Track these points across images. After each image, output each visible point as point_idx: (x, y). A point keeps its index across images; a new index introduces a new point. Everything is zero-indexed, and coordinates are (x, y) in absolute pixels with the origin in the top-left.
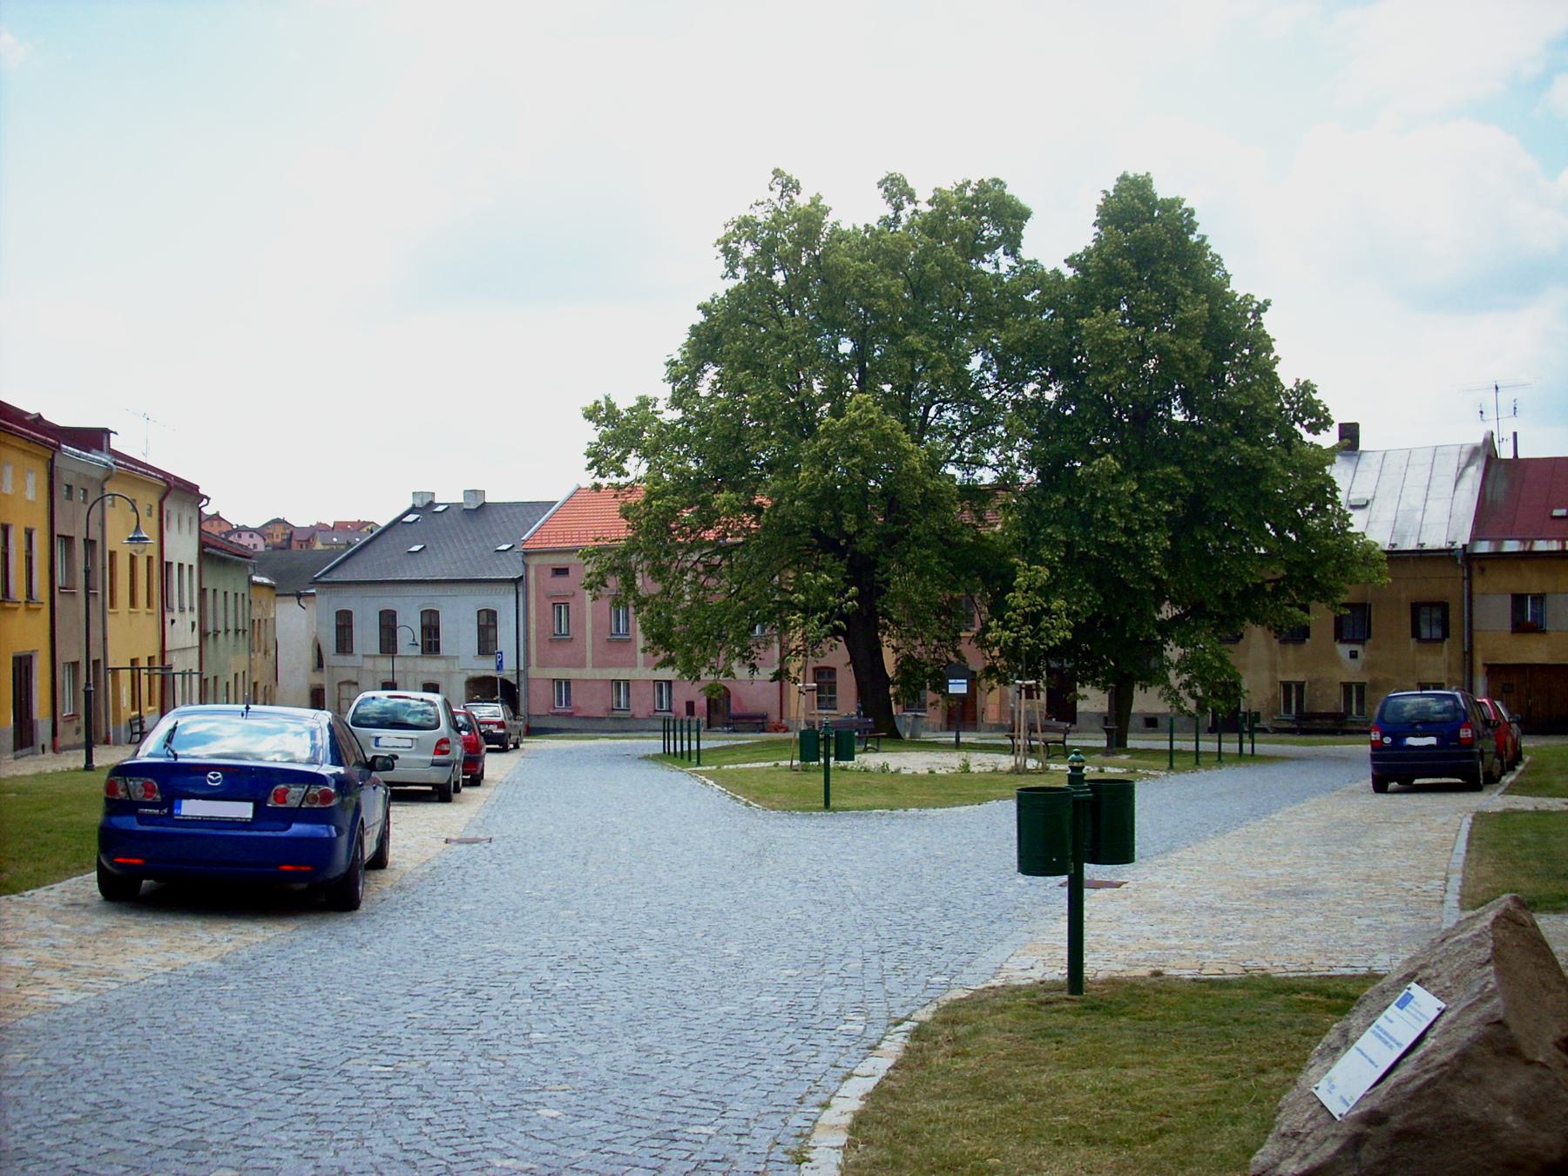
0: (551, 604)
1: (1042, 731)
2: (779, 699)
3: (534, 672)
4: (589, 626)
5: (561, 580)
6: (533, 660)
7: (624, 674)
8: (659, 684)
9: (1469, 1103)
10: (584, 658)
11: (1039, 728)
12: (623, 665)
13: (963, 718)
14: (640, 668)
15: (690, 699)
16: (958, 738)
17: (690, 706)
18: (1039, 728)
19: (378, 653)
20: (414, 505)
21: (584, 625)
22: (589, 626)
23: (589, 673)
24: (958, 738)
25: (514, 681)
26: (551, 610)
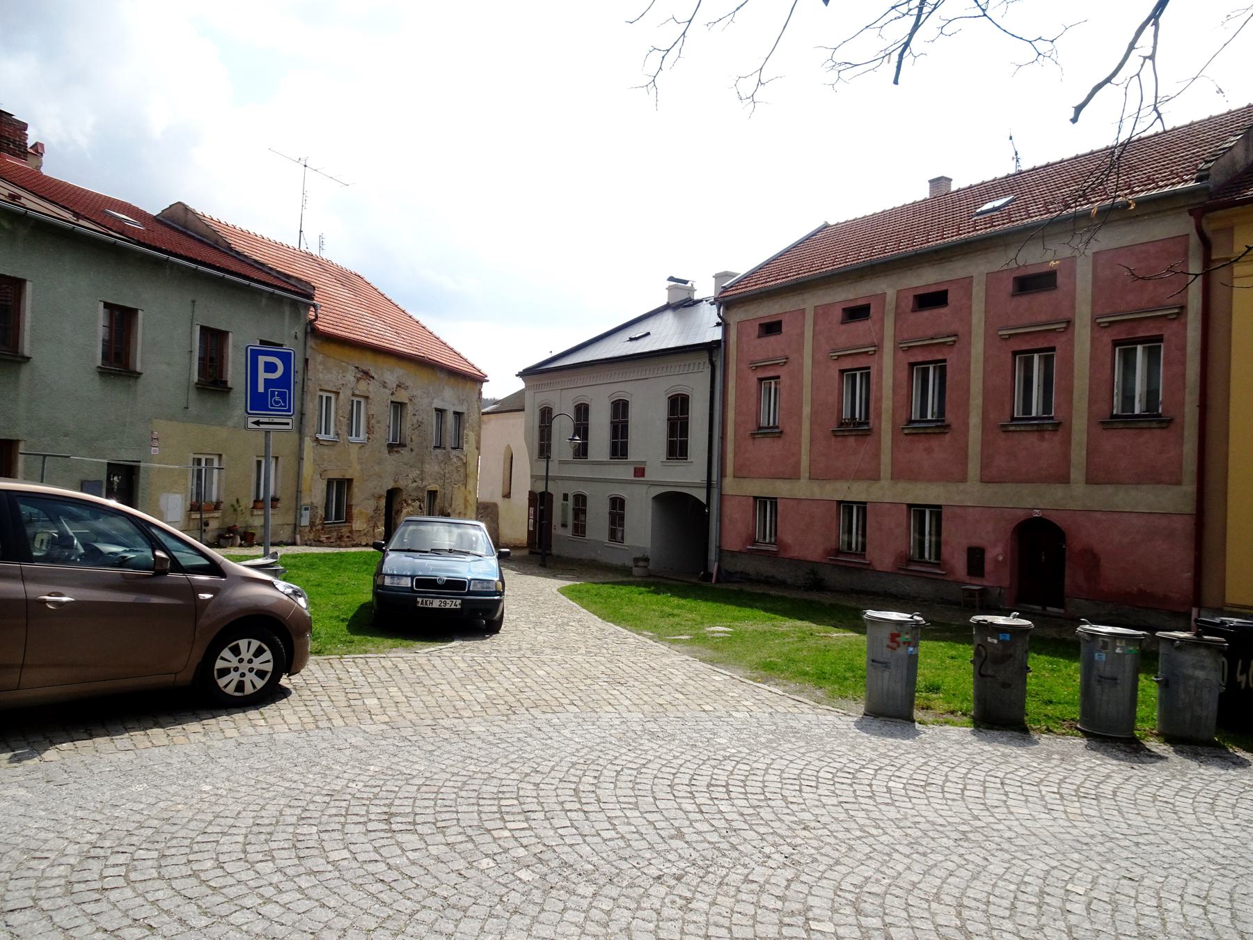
0: (755, 380)
1: (1090, 480)
2: (1191, 558)
3: (730, 485)
4: (807, 410)
5: (860, 327)
6: (730, 469)
7: (857, 492)
8: (917, 511)
9: (190, 213)
10: (797, 466)
11: (805, 473)
12: (859, 476)
13: (545, 411)
14: (885, 482)
15: (976, 542)
16: (201, 516)
17: (976, 558)
18: (805, 473)
19: (570, 459)
20: (668, 303)
21: (801, 408)
22: (807, 410)
23: (802, 488)
24: (201, 516)
25: (701, 495)
26: (754, 390)
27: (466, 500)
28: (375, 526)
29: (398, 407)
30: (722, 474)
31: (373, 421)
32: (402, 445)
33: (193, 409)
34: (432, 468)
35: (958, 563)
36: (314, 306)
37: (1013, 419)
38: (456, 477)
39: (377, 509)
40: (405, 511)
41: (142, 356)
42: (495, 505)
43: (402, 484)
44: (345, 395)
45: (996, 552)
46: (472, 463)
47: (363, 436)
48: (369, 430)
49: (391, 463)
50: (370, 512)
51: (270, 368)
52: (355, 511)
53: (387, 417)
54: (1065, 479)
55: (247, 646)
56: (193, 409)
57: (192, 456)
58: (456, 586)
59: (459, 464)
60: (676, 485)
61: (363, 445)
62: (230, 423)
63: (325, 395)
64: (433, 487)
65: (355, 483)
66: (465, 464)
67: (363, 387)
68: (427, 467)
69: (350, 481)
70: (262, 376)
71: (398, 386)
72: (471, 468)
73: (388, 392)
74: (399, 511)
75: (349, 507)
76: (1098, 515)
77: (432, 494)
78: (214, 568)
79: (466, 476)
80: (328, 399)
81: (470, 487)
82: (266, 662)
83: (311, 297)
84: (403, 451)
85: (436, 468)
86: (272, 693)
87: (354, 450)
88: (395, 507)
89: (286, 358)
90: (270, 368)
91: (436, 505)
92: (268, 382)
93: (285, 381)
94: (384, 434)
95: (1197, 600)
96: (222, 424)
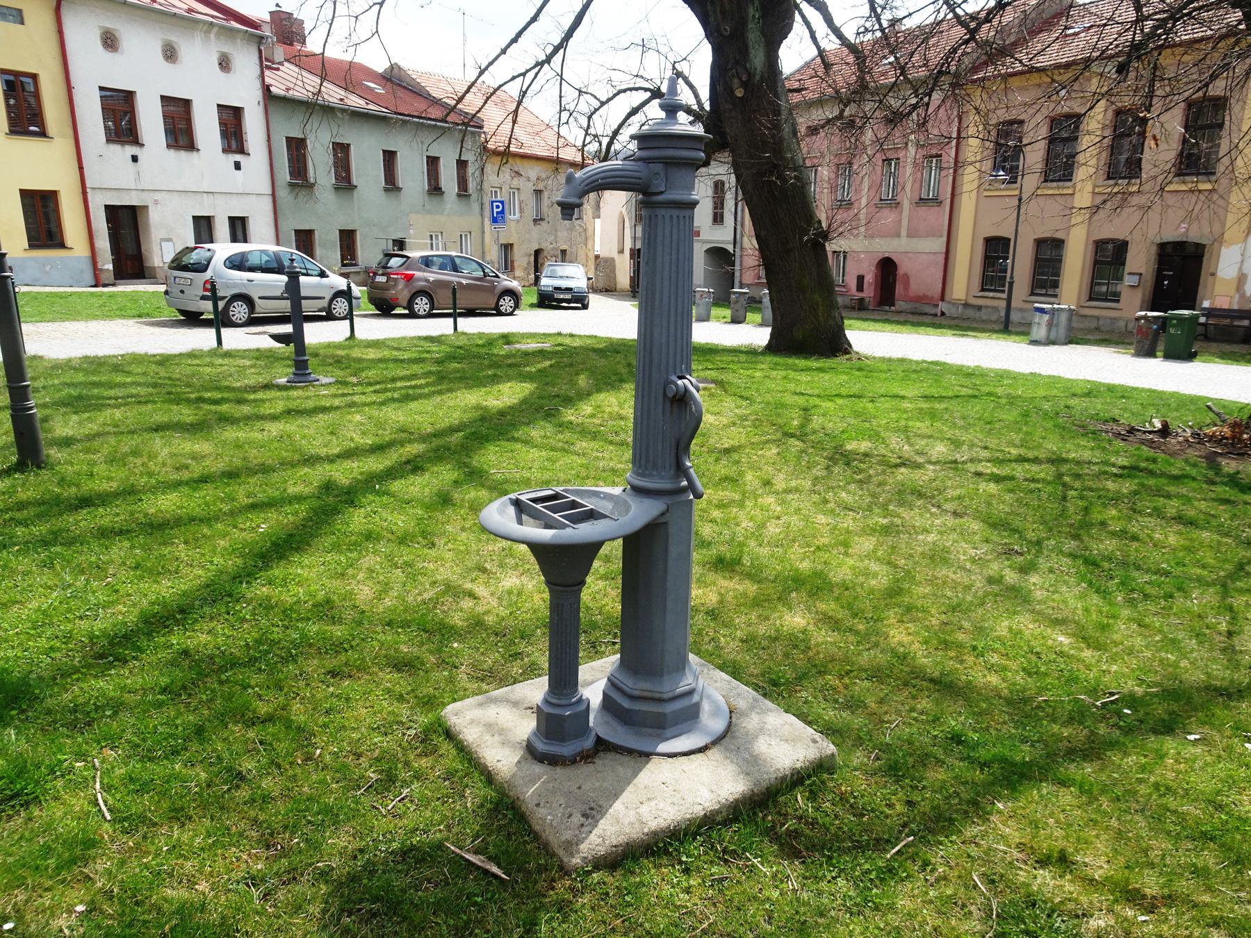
15: (861, 273)
25: (730, 248)
27: (587, 256)
28: (529, 274)
29: (538, 193)
30: (742, 236)
31: (523, 205)
32: (542, 219)
33: (427, 206)
34: (563, 234)
35: (853, 284)
36: (484, 133)
37: (881, 200)
38: (579, 239)
39: (529, 263)
40: (547, 264)
41: (402, 179)
42: (613, 260)
43: (543, 246)
44: (505, 189)
45: (869, 278)
46: (590, 229)
47: (518, 215)
48: (521, 211)
49: (536, 231)
50: (525, 265)
51: (498, 207)
52: (516, 264)
53: (531, 201)
54: (898, 235)
55: (507, 298)
56: (427, 206)
57: (429, 234)
58: (569, 290)
59: (581, 230)
60: (718, 242)
61: (518, 221)
62: (446, 212)
63: (493, 190)
64: (564, 247)
65: (515, 247)
66: (585, 230)
67: (515, 183)
68: (559, 234)
69: (512, 245)
70: (495, 210)
71: (538, 179)
72: (590, 233)
73: (532, 184)
74: (542, 264)
75: (512, 262)
76: (910, 255)
77: (564, 252)
78: (497, 276)
79: (586, 238)
80: (496, 192)
81: (589, 246)
82: (512, 303)
83: (481, 127)
84: (543, 223)
85: (565, 234)
86: (511, 314)
87: (513, 224)
88: (540, 261)
89: (502, 202)
90: (498, 207)
91: (564, 256)
92: (497, 213)
93: (503, 212)
94: (530, 213)
95: (942, 299)
96: (442, 214)
